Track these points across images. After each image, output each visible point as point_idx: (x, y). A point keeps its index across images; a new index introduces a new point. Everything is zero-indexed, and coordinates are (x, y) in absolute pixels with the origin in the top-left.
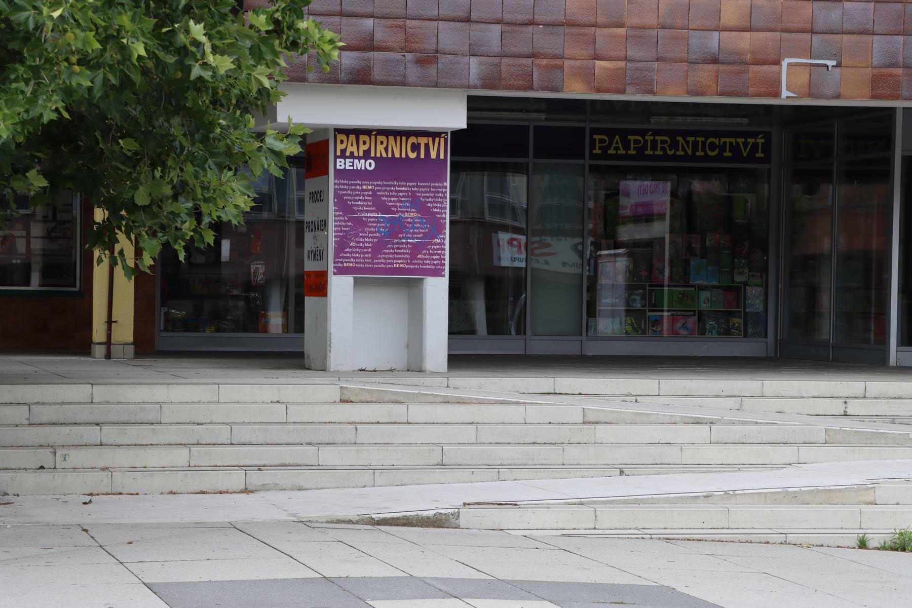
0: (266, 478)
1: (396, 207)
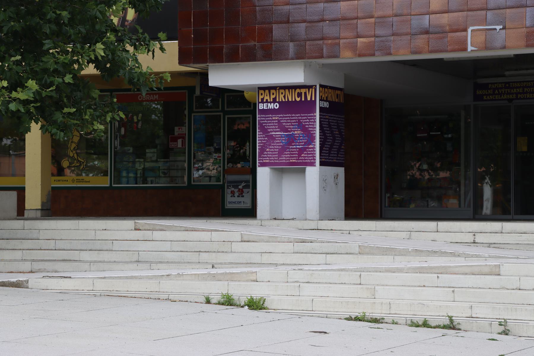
0: (41, 265)
1: (290, 128)
